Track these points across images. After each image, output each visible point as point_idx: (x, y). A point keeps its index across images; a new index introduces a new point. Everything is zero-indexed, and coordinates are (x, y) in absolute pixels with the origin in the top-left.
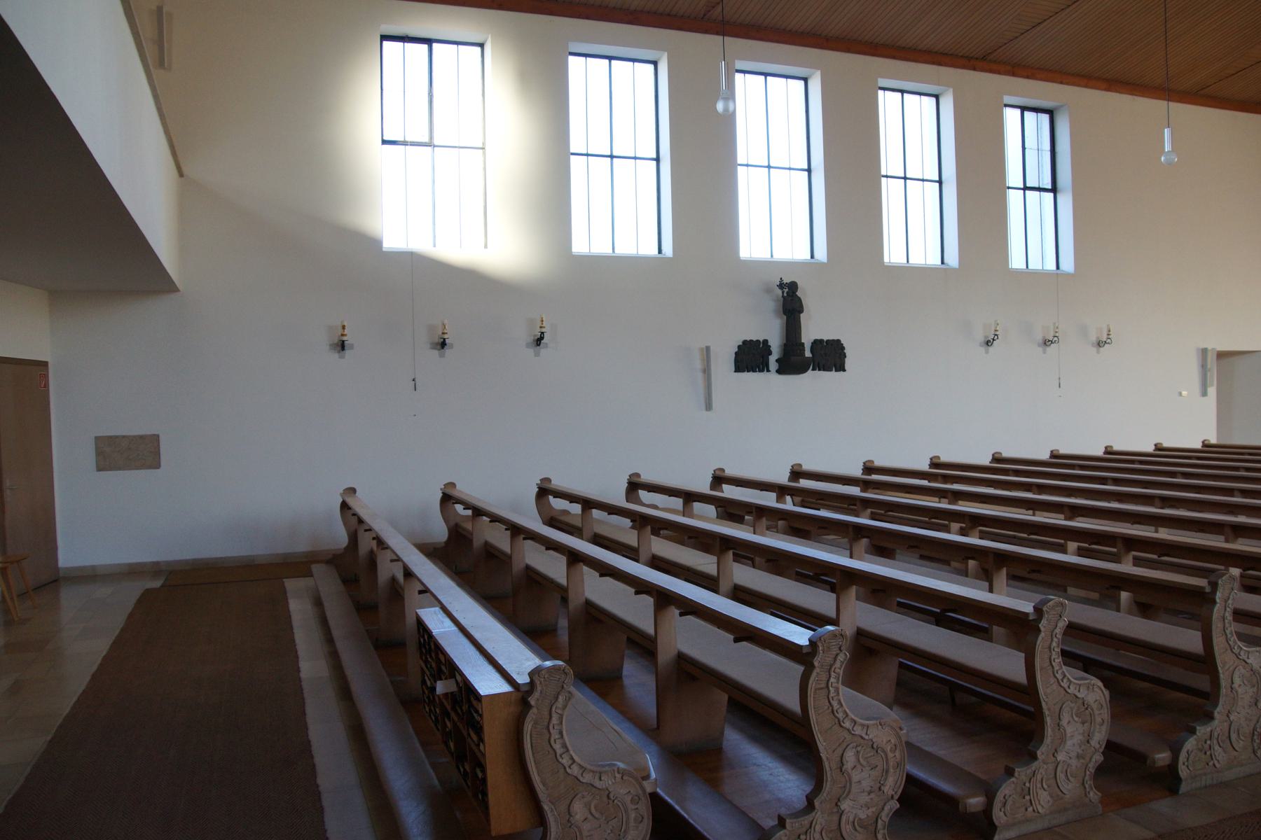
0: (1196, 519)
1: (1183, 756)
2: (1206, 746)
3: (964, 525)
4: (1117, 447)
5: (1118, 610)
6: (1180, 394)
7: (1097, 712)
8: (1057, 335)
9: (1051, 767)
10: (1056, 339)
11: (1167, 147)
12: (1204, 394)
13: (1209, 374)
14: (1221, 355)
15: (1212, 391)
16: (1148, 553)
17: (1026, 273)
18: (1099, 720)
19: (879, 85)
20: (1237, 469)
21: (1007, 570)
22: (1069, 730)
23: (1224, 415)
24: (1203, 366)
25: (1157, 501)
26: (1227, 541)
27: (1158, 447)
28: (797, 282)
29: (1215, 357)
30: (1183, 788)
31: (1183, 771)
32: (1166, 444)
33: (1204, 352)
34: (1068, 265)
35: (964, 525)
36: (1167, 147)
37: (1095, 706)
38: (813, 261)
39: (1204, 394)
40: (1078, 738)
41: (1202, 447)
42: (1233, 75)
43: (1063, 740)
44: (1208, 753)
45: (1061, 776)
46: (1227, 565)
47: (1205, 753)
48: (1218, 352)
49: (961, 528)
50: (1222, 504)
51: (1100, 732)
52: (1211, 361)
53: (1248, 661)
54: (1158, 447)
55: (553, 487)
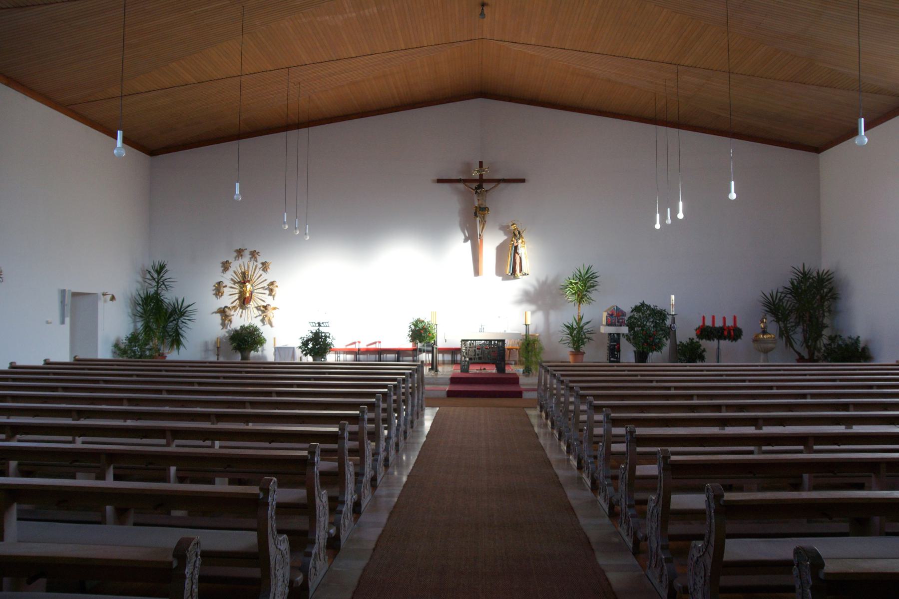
0: (251, 414)
3: (386, 425)
4: (20, 363)
11: (237, 192)
12: (63, 322)
13: (66, 307)
14: (75, 295)
15: (67, 320)
16: (89, 436)
19: (828, 328)
20: (131, 376)
24: (62, 302)
25: (248, 405)
26: (213, 424)
27: (47, 362)
32: (52, 360)
33: (63, 292)
35: (386, 425)
36: (237, 192)
39: (63, 322)
41: (74, 361)
42: (93, 101)
46: (213, 440)
48: (72, 292)
50: (215, 401)
54: (47, 362)
55: (337, 425)
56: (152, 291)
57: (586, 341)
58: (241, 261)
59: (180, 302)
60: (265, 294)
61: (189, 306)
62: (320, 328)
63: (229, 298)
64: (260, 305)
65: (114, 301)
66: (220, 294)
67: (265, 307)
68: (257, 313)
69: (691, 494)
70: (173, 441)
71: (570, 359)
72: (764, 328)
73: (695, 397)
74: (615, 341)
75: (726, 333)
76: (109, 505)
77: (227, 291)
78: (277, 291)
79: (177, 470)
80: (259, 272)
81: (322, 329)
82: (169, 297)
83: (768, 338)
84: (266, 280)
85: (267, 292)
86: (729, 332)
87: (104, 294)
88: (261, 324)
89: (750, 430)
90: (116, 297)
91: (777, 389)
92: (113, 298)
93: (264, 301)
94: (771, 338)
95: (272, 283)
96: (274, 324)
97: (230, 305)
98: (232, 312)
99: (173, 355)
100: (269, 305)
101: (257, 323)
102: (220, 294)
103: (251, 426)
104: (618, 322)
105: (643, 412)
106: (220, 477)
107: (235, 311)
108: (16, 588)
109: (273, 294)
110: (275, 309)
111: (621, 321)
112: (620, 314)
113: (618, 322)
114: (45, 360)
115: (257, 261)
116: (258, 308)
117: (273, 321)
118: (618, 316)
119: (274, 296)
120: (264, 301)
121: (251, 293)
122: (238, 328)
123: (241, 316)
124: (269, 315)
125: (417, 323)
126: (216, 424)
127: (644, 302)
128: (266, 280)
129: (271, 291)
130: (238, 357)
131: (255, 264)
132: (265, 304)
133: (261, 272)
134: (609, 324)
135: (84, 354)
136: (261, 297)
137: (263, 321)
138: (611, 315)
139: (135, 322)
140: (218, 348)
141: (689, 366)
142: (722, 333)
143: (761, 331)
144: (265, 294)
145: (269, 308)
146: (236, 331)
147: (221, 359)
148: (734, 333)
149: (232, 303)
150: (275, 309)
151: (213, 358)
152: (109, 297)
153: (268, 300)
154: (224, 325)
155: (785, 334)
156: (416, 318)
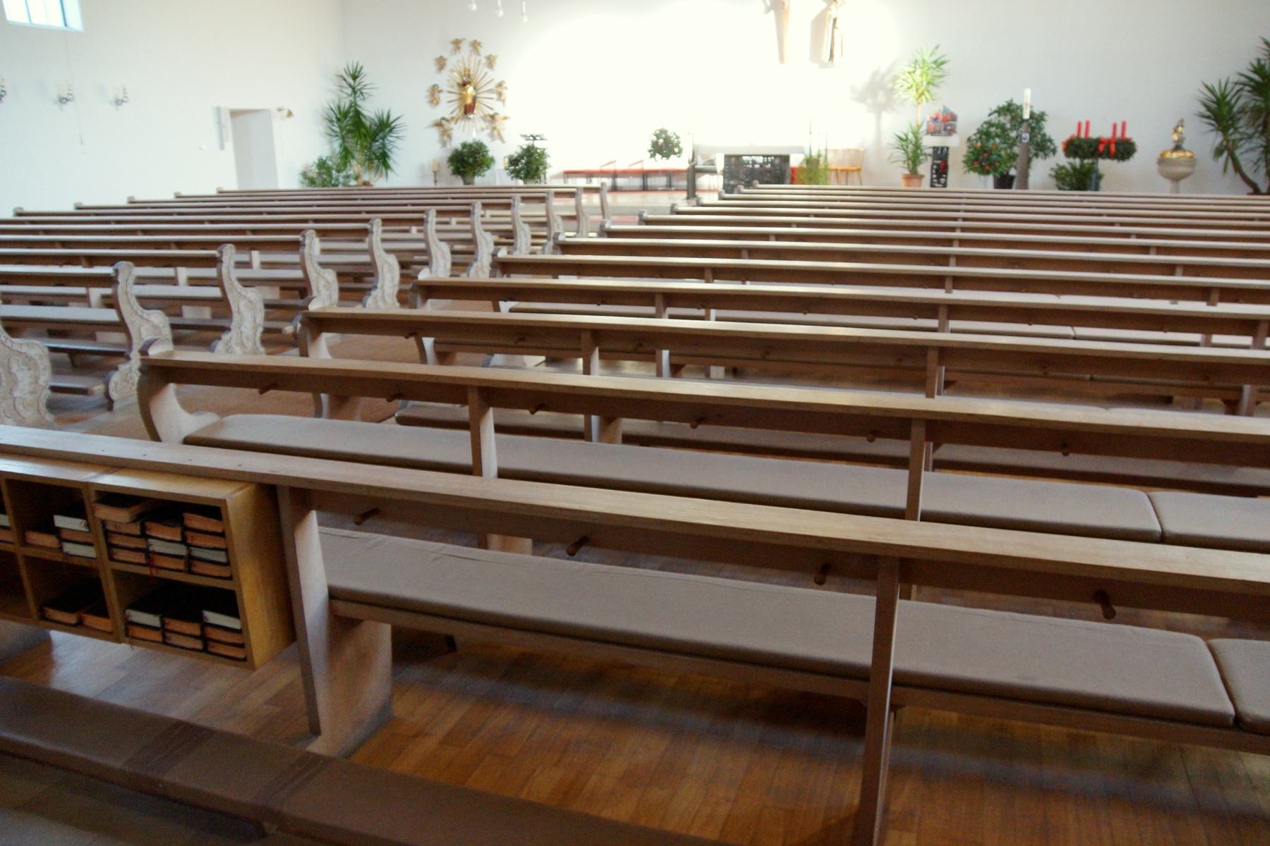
1: (112, 386)
2: (128, 378)
5: (90, 306)
6: (201, 149)
7: (39, 362)
8: (71, 93)
9: (11, 401)
10: (70, 96)
12: (222, 147)
14: (235, 114)
15: (229, 145)
17: (64, 32)
18: (41, 367)
21: (1117, 605)
22: (20, 375)
23: (242, 169)
28: (1132, 160)
29: (228, 116)
30: (116, 406)
31: (114, 395)
32: (184, 193)
33: (218, 110)
34: (76, 22)
37: (36, 358)
38: (65, 29)
39: (222, 147)
40: (28, 380)
43: (15, 382)
44: (130, 382)
45: (20, 407)
47: (128, 382)
49: (104, 297)
51: (44, 375)
52: (227, 119)
53: (150, 319)
56: (346, 103)
57: (923, 160)
58: (459, 56)
59: (385, 117)
60: (492, 99)
61: (398, 118)
62: (535, 142)
63: (447, 107)
64: (486, 113)
65: (292, 118)
66: (435, 101)
67: (493, 117)
68: (483, 124)
69: (1161, 410)
70: (665, 309)
71: (902, 185)
72: (1178, 141)
73: (956, 243)
74: (940, 159)
75: (1101, 148)
76: (595, 414)
77: (444, 97)
78: (507, 94)
79: (671, 354)
80: (483, 69)
81: (538, 144)
82: (371, 110)
83: (1180, 157)
84: (492, 80)
85: (495, 96)
86: (1108, 148)
87: (280, 110)
88: (489, 139)
89: (1199, 307)
90: (294, 113)
91: (777, 240)
92: (290, 114)
93: (491, 109)
94: (1184, 157)
95: (500, 85)
96: (505, 139)
97: (448, 116)
98: (452, 125)
99: (380, 183)
100: (496, 114)
101: (484, 138)
102: (435, 101)
103: (750, 287)
104: (945, 129)
105: (1198, 275)
106: (187, 305)
107: (456, 123)
108: (505, 548)
109: (502, 98)
110: (505, 118)
111: (949, 128)
112: (949, 118)
113: (945, 129)
114: (175, 194)
115: (479, 55)
116: (484, 118)
117: (504, 134)
118: (945, 120)
119: (504, 101)
120: (491, 109)
121: (474, 99)
122: (459, 148)
123: (463, 131)
124: (498, 127)
125: (662, 133)
126: (713, 282)
127: (1012, 101)
128: (492, 80)
129: (500, 94)
130: (459, 183)
131: (478, 58)
132: (492, 113)
133: (486, 70)
134: (933, 132)
135: (259, 184)
136: (488, 104)
137: (491, 135)
138: (935, 120)
139: (331, 142)
140: (435, 173)
141: (1076, 195)
142: (1097, 149)
143: (1172, 146)
144: (492, 99)
145: (497, 117)
146: (456, 151)
147: (439, 185)
148: (1116, 148)
149: (452, 113)
150: (505, 118)
151: (432, 185)
152: (285, 112)
153: (497, 107)
154: (444, 144)
155: (1226, 150)
156: (660, 127)
